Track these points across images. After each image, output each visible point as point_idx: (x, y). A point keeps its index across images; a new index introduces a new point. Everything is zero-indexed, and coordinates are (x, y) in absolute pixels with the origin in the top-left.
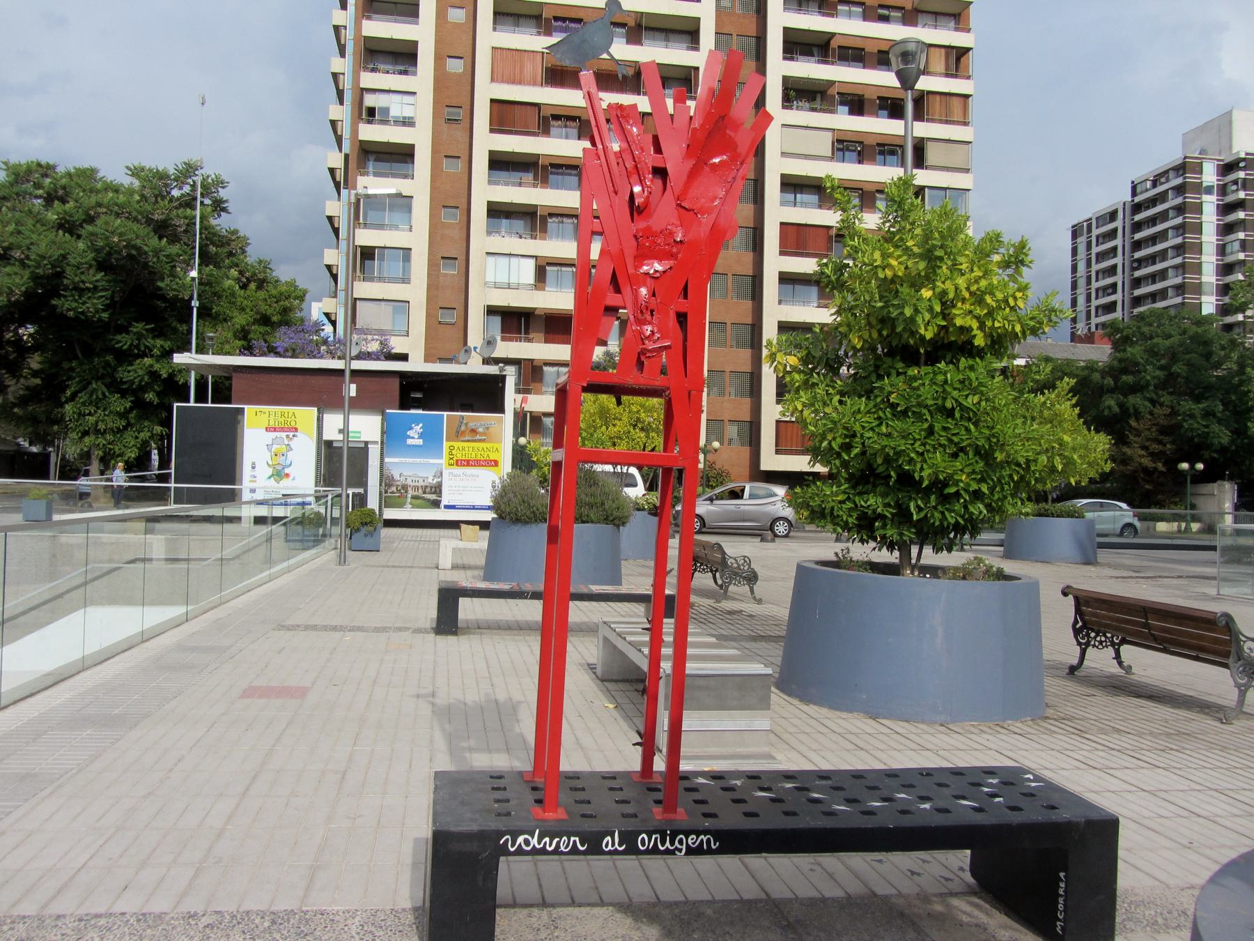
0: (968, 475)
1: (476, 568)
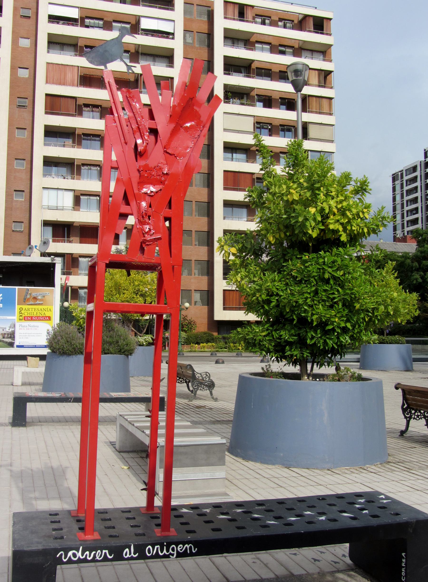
0: (339, 318)
1: (37, 384)
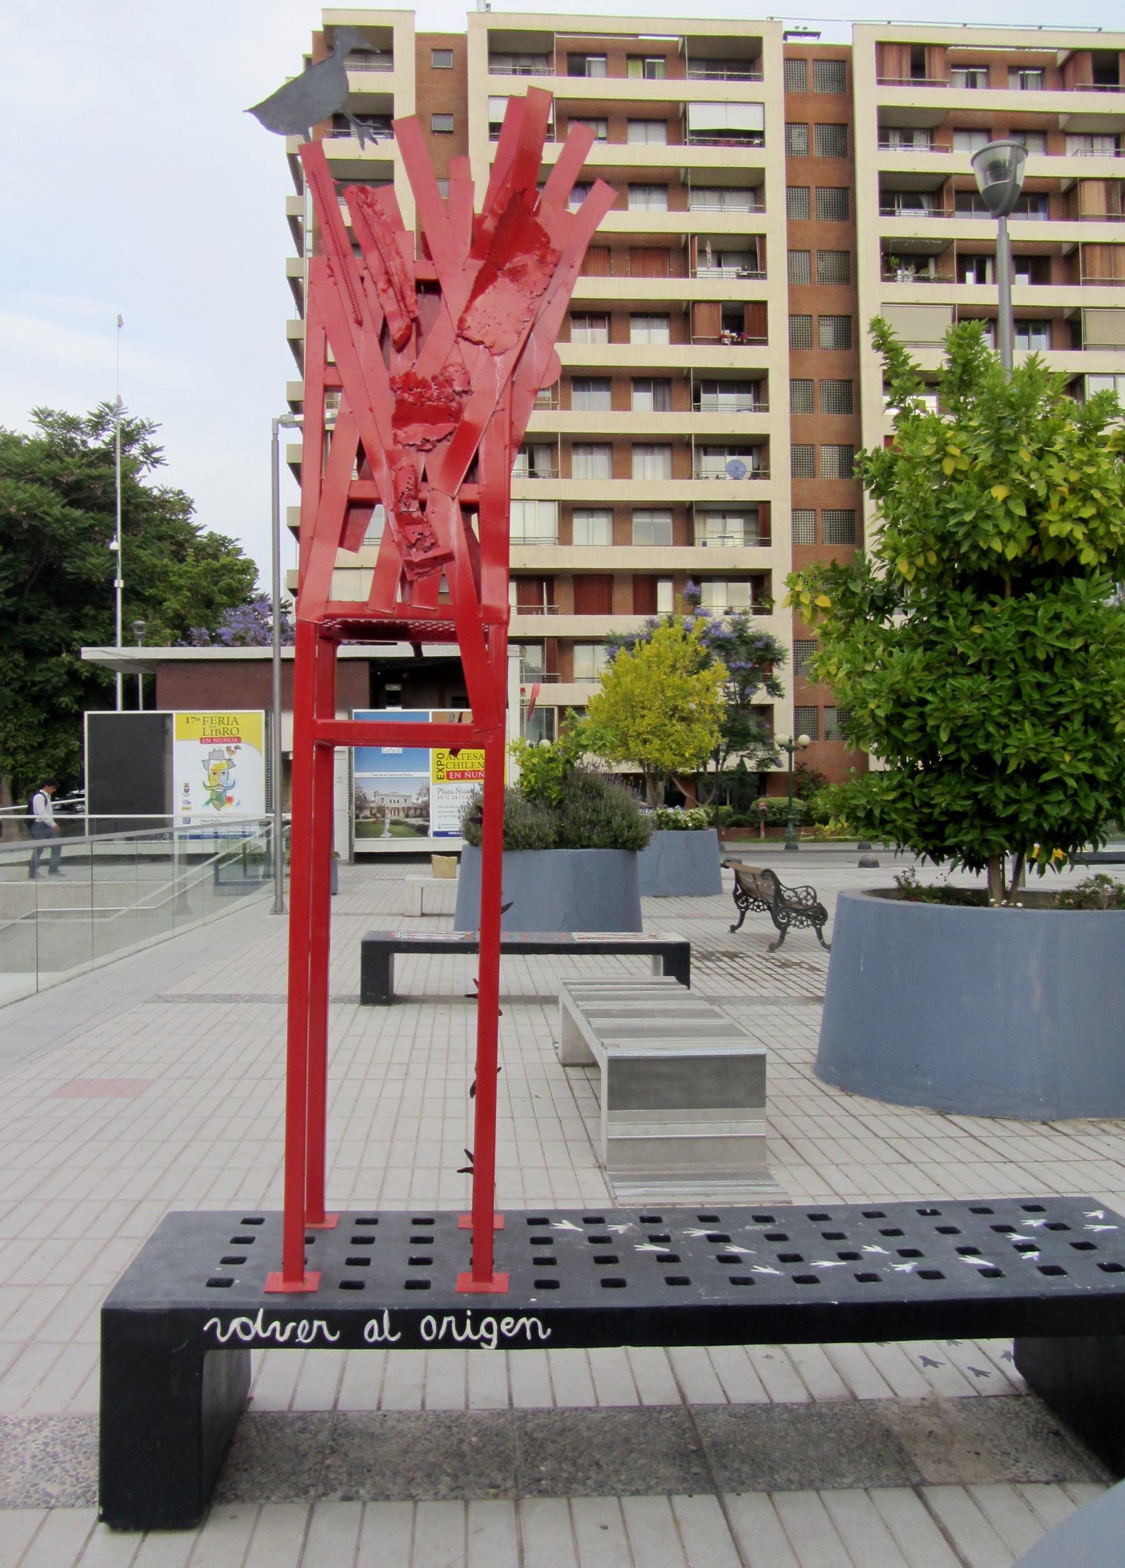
0: (1076, 753)
